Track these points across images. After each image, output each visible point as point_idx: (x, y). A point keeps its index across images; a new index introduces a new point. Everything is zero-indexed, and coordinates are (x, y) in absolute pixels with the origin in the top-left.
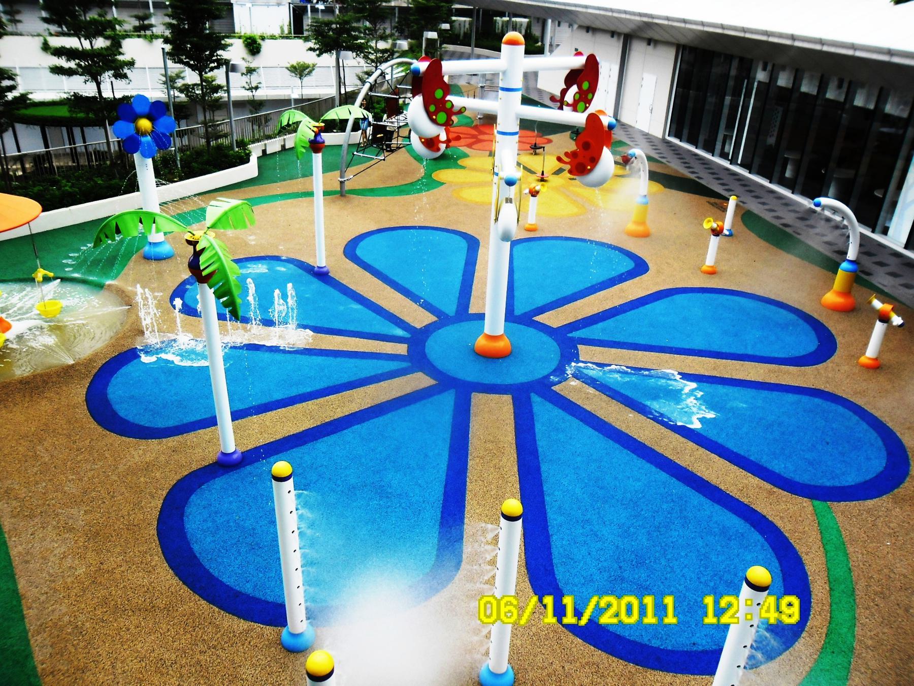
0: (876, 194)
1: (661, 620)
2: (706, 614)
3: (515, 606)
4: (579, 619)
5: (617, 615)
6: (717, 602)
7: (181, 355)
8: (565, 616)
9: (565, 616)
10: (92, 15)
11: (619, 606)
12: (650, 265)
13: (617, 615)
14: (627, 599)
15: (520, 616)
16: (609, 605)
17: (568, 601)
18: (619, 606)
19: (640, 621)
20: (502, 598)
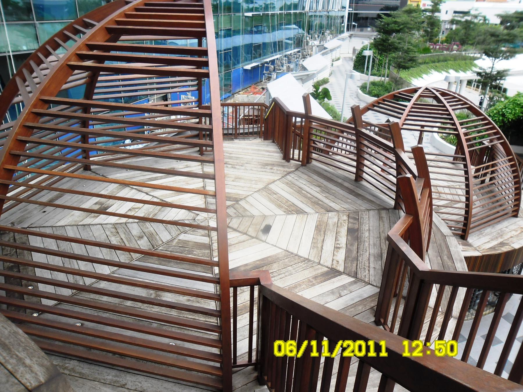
0: (102, 2)
1: (378, 354)
2: (312, 351)
3: (294, 346)
4: (332, 354)
5: (353, 352)
6: (410, 345)
7: (320, 231)
8: (369, 352)
9: (369, 352)
10: (454, 27)
11: (354, 346)
12: (332, 98)
13: (353, 352)
14: (359, 342)
15: (298, 351)
16: (349, 346)
17: (371, 343)
18: (354, 346)
19: (366, 355)
20: (448, 342)
